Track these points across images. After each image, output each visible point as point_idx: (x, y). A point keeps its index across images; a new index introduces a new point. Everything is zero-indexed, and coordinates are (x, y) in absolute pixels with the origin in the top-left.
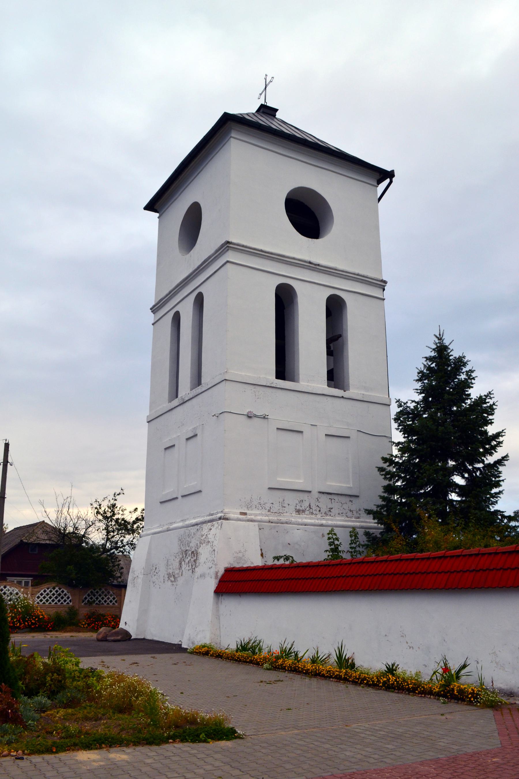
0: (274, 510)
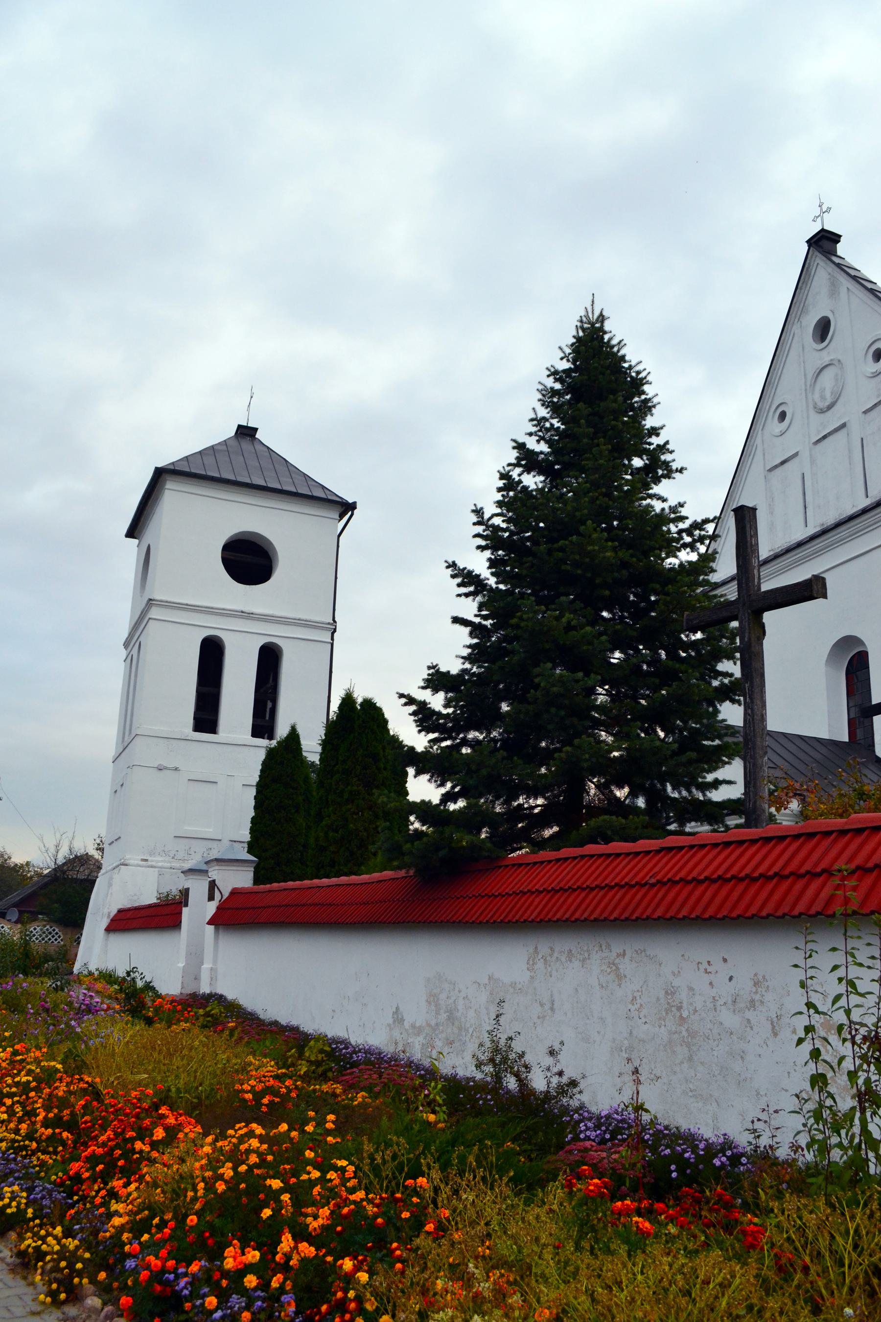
0: (178, 857)
